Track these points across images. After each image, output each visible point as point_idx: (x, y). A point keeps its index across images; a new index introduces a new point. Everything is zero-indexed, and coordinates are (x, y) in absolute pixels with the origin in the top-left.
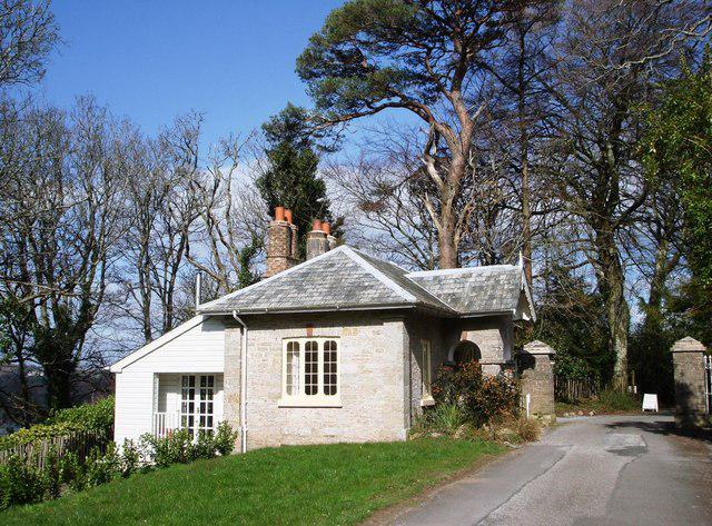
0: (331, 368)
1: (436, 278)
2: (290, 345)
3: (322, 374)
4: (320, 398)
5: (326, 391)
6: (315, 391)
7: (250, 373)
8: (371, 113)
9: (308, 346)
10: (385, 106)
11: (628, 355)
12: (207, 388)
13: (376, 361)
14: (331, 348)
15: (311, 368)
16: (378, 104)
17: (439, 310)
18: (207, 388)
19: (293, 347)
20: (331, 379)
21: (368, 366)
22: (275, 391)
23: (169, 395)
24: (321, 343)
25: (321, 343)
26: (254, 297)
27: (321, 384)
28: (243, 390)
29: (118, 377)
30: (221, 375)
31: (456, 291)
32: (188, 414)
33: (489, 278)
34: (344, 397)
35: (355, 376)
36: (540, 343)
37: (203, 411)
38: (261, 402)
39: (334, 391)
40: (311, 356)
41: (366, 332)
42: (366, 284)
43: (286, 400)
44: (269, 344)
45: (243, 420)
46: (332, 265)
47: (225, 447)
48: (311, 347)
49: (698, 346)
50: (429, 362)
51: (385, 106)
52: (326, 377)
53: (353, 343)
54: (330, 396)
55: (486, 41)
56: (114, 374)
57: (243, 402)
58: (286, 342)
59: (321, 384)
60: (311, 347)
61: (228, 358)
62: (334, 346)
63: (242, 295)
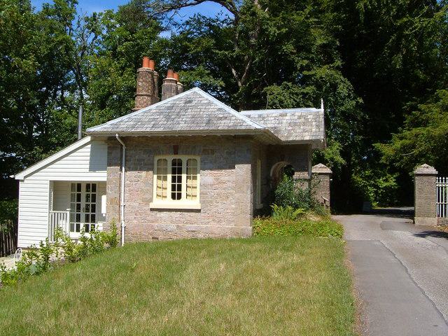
1: (260, 116)
23: (243, 171)
26: (132, 123)
28: (122, 194)
29: (21, 184)
30: (104, 183)
31: (276, 125)
32: (76, 193)
33: (300, 117)
36: (323, 165)
37: (87, 210)
38: (136, 204)
39: (179, 197)
42: (221, 116)
44: (144, 160)
45: (122, 218)
46: (190, 102)
47: (113, 242)
49: (433, 170)
54: (176, 201)
56: (18, 181)
57: (122, 204)
63: (121, 121)
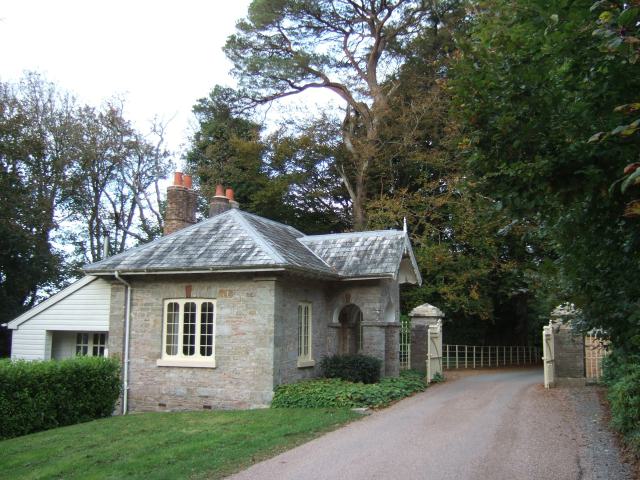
0: (207, 329)
2: (170, 305)
3: (199, 334)
4: (197, 359)
5: (185, 351)
6: (192, 352)
7: (133, 332)
8: (296, 92)
9: (187, 307)
10: (306, 86)
11: (446, 328)
12: (99, 346)
13: (247, 322)
14: (208, 308)
15: (189, 329)
16: (303, 84)
17: (325, 274)
18: (99, 346)
19: (174, 307)
20: (206, 340)
21: (242, 328)
22: (156, 351)
24: (199, 303)
25: (199, 303)
27: (197, 345)
34: (218, 359)
35: (229, 337)
39: (209, 354)
40: (189, 317)
41: (240, 292)
43: (167, 359)
44: (151, 304)
48: (190, 308)
50: (310, 325)
51: (306, 86)
52: (203, 338)
53: (135, 297)
55: (576, 69)
56: (11, 330)
58: (167, 302)
59: (197, 345)
60: (190, 308)
61: (113, 318)
62: (211, 308)
